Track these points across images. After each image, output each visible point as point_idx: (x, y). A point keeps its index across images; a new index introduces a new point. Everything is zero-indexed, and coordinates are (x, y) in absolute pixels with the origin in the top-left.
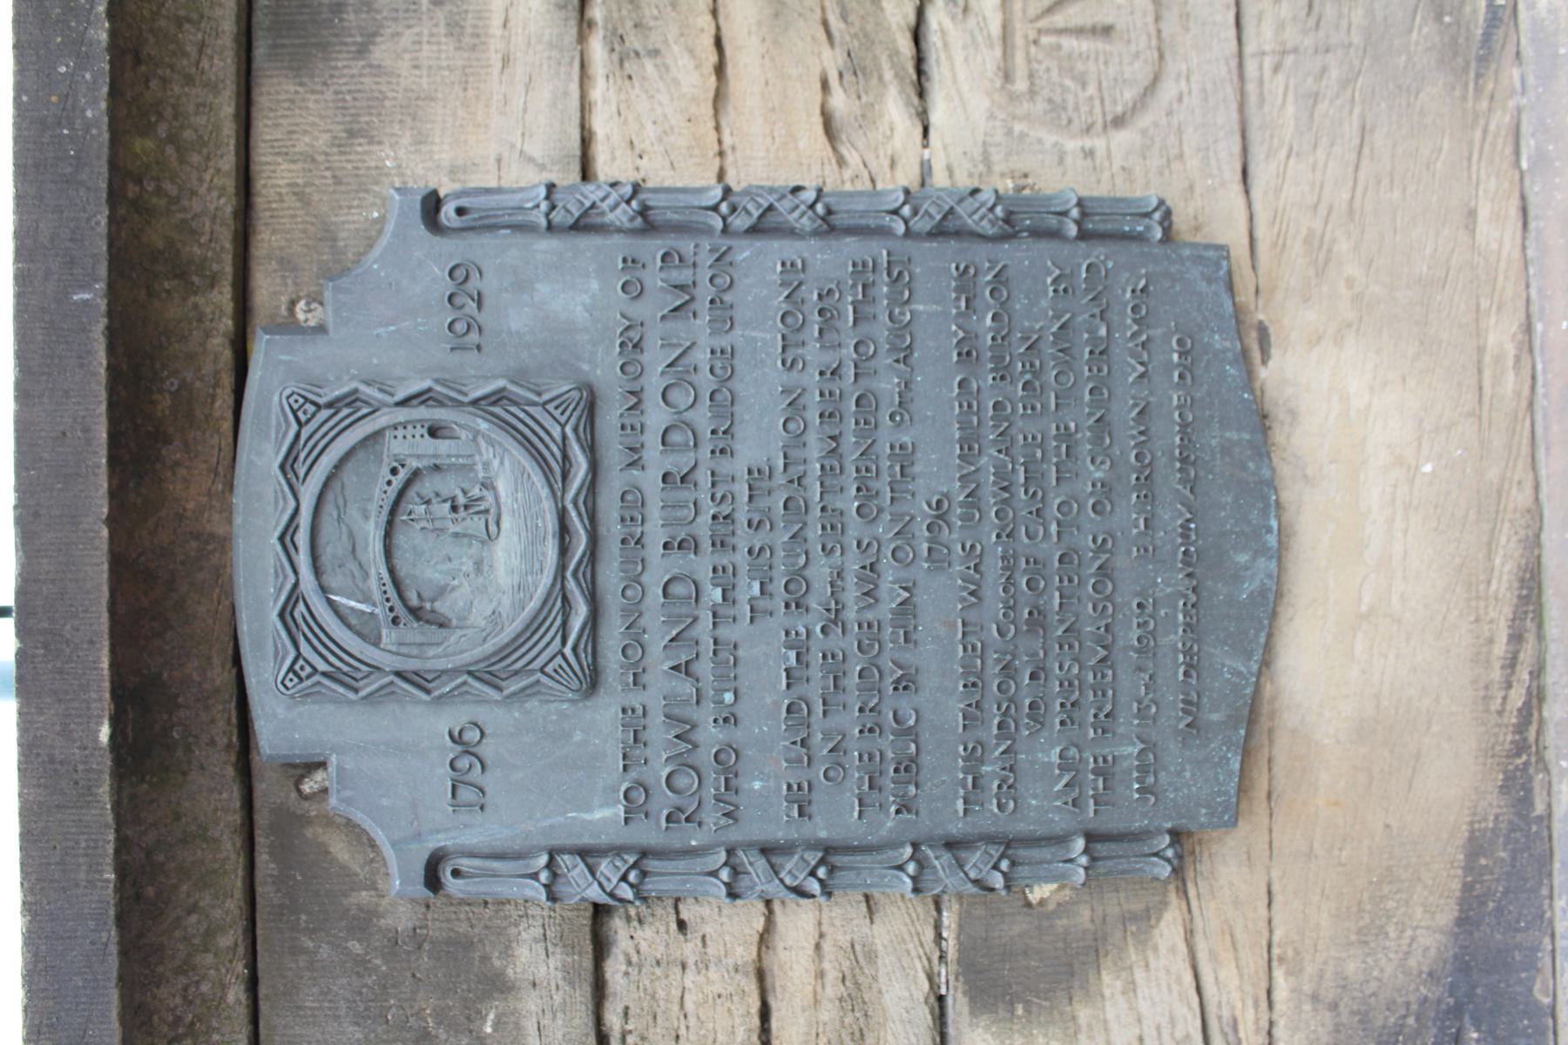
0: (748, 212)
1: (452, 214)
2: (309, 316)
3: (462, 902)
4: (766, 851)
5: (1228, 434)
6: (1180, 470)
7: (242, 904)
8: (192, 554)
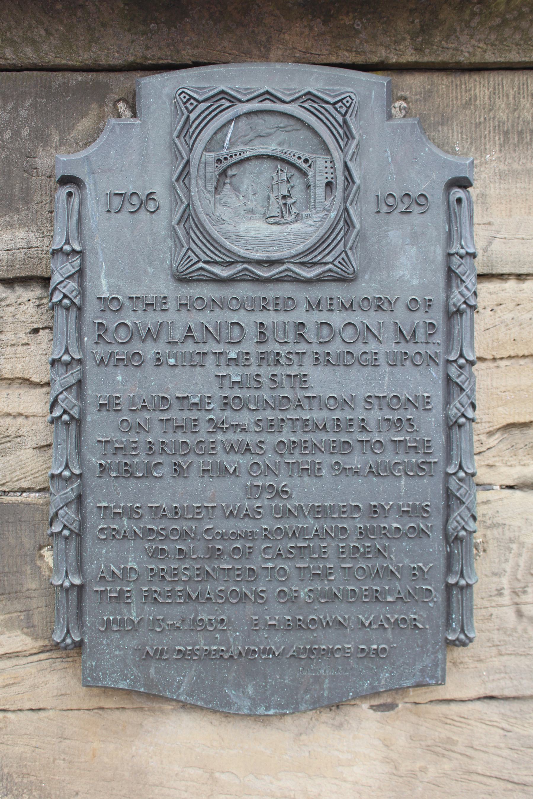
0: (459, 376)
1: (457, 196)
2: (398, 109)
3: (52, 198)
4: (80, 383)
5: (327, 681)
6: (305, 648)
7: (52, 63)
8: (259, 38)
